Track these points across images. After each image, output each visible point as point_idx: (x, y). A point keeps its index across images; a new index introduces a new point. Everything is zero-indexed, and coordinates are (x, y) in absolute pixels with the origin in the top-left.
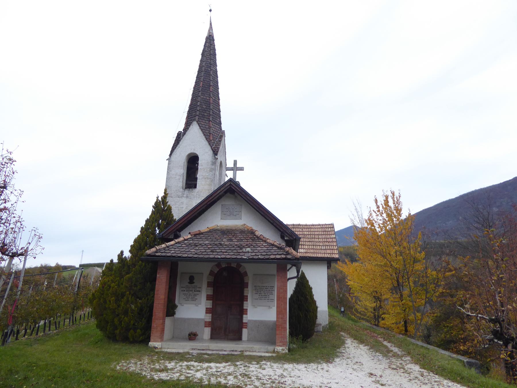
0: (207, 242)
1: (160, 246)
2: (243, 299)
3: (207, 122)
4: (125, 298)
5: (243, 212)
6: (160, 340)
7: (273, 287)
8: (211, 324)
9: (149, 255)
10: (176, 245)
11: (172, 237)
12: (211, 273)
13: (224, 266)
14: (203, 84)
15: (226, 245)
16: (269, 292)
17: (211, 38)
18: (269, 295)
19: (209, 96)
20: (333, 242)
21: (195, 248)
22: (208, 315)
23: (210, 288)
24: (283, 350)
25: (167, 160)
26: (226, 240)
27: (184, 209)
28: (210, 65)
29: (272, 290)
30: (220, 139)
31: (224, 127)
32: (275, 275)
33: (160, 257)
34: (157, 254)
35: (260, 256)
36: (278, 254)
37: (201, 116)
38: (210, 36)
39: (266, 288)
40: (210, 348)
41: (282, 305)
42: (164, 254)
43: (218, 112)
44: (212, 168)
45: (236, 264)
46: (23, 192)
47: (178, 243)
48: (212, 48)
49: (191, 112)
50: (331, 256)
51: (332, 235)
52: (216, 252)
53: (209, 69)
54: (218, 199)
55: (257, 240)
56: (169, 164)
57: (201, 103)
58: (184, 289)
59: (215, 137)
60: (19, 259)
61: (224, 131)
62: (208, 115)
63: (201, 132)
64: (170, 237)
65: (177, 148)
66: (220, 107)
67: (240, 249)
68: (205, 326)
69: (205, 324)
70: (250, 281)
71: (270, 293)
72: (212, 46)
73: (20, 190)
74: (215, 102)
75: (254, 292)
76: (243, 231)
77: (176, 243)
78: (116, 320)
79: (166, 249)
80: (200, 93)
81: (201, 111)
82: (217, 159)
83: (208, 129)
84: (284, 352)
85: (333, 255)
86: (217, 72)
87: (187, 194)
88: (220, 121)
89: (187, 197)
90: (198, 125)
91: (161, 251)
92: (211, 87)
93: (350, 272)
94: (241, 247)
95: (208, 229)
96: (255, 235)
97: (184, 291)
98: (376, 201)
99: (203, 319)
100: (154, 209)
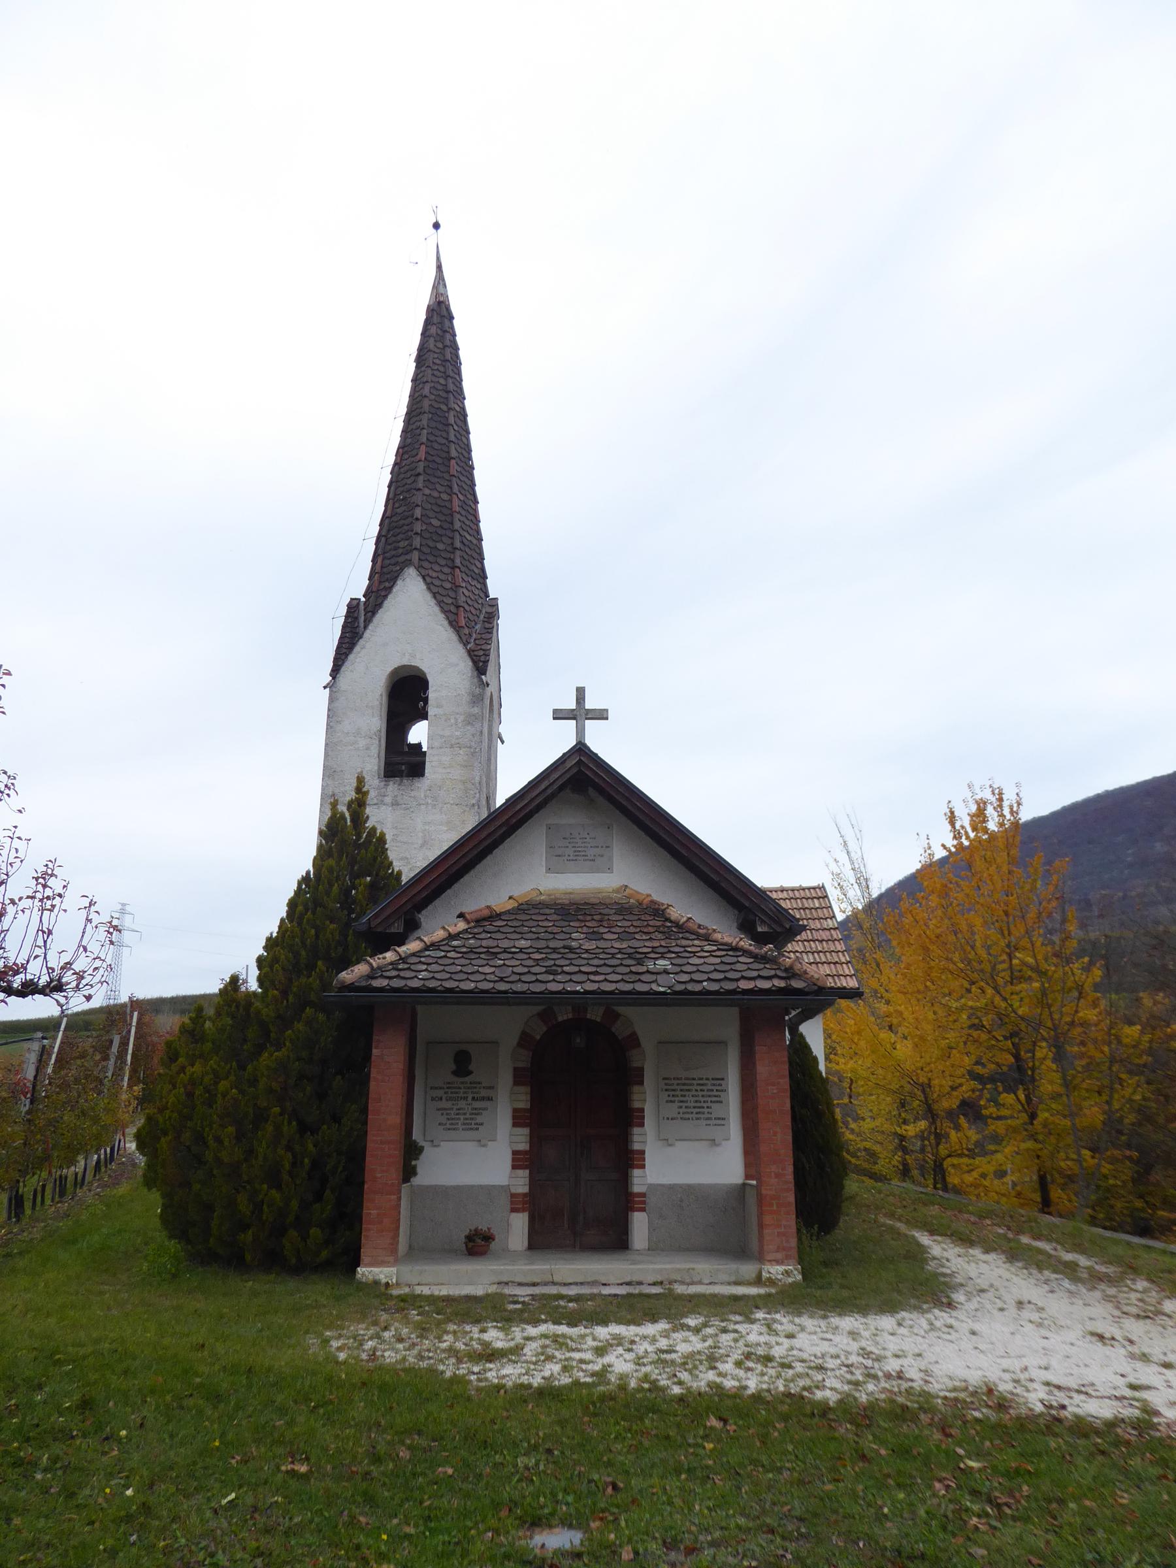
0: (523, 943)
1: (381, 956)
2: (630, 1118)
3: (446, 570)
4: (270, 1128)
5: (615, 850)
6: (391, 1259)
7: (723, 1079)
8: (530, 1203)
9: (352, 987)
10: (427, 953)
12: (525, 1040)
13: (565, 1018)
15: (587, 951)
16: (710, 1096)
17: (445, 313)
18: (709, 1104)
19: (449, 491)
20: (833, 941)
21: (491, 963)
22: (520, 1172)
23: (522, 1089)
24: (789, 1276)
26: (582, 936)
28: (444, 395)
30: (487, 625)
31: (494, 588)
33: (405, 991)
34: (377, 983)
35: (705, 984)
36: (760, 977)
38: (440, 303)
39: (698, 1085)
40: (557, 1279)
41: (775, 1134)
42: (396, 983)
43: (475, 541)
45: (601, 1010)
46: (15, 778)
48: (448, 343)
49: (394, 539)
50: (836, 983)
51: (826, 919)
52: (563, 972)
53: (444, 408)
55: (681, 935)
56: (332, 700)
58: (440, 1093)
59: (471, 617)
60: (57, 1001)
61: (497, 599)
62: (449, 549)
63: (433, 602)
66: (481, 524)
67: (639, 964)
68: (513, 1210)
69: (512, 1203)
70: (649, 1063)
71: (714, 1099)
72: (448, 336)
73: (5, 773)
75: (664, 1096)
76: (627, 906)
77: (427, 948)
78: (242, 1201)
79: (400, 967)
80: (421, 478)
81: (427, 535)
82: (488, 685)
83: (452, 594)
84: (790, 1280)
85: (840, 980)
86: (465, 416)
88: (483, 570)
89: (395, 804)
90: (420, 579)
91: (384, 974)
92: (453, 462)
93: (846, 1033)
94: (638, 956)
95: (511, 901)
96: (668, 920)
98: (952, 819)
99: (502, 1187)
100: (324, 842)
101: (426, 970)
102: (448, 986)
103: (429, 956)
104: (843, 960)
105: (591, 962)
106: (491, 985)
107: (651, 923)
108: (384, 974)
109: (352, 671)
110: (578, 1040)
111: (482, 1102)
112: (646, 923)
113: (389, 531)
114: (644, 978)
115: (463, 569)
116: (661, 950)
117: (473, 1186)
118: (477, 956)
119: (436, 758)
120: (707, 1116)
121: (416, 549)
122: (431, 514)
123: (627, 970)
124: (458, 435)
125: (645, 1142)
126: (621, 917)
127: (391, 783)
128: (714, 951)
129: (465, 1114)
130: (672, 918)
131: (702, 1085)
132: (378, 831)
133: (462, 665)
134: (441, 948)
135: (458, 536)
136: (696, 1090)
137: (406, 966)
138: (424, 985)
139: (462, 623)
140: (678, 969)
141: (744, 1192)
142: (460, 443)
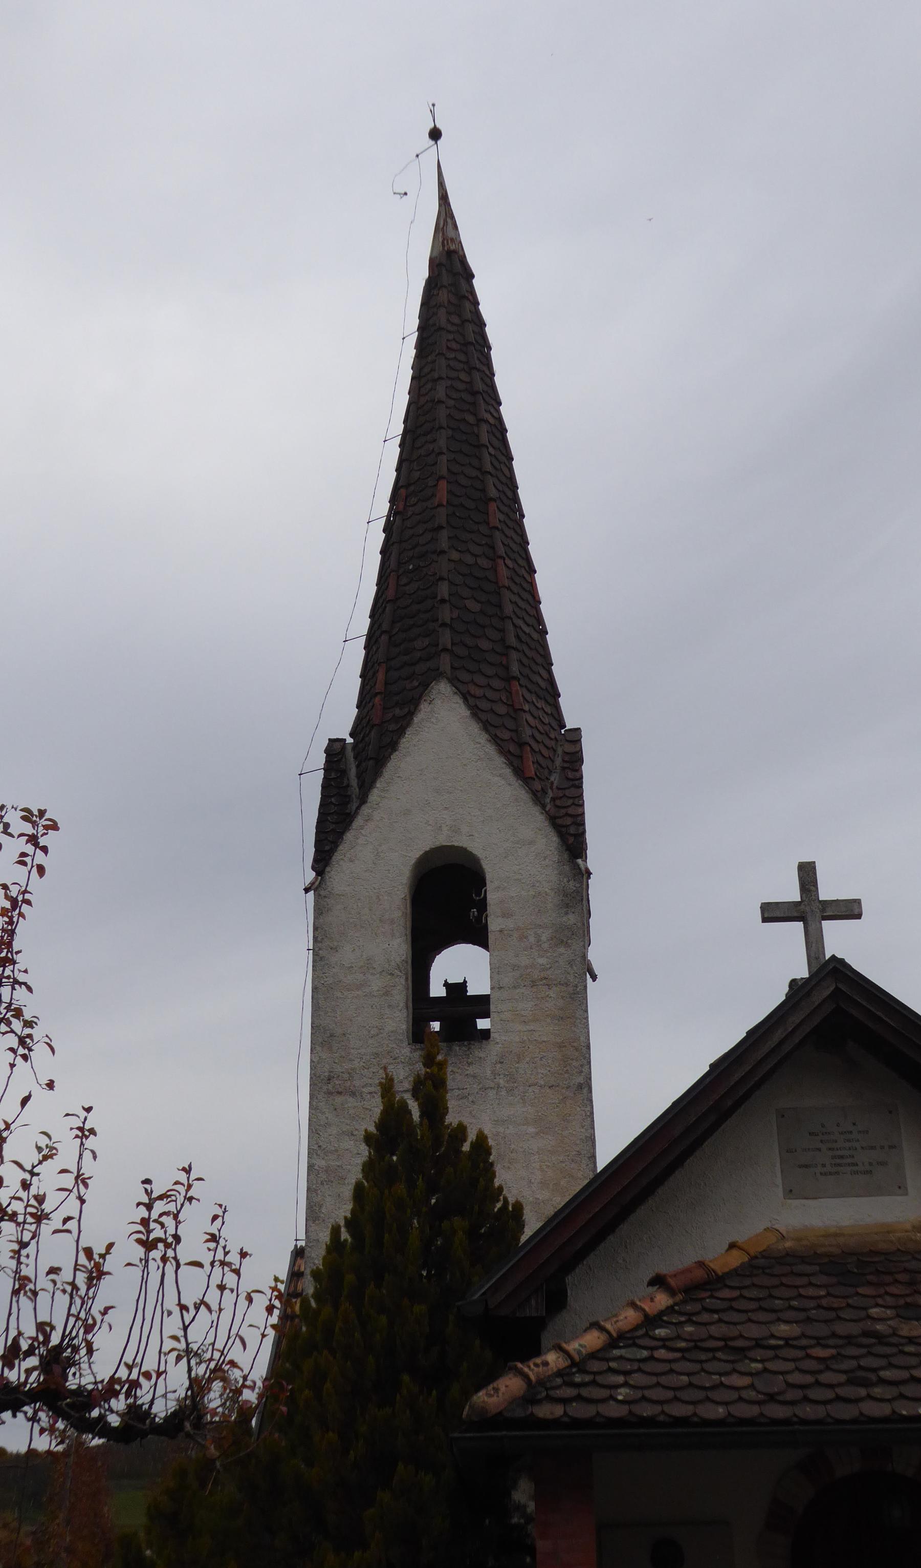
1: (538, 1361)
3: (497, 683)
10: (616, 1352)
14: (450, 492)
25: (307, 890)
34: (545, 1411)
43: (535, 636)
48: (469, 316)
53: (471, 419)
56: (319, 911)
61: (577, 731)
63: (483, 738)
72: (467, 305)
74: (517, 580)
80: (444, 534)
83: (510, 724)
90: (458, 699)
95: (735, 1252)
101: (626, 1384)
103: (621, 1358)
106: (657, 1409)
108: (552, 1393)
109: (351, 861)
113: (393, 622)
115: (523, 681)
118: (710, 1355)
121: (445, 650)
124: (496, 463)
132: (472, 1136)
134: (639, 1342)
135: (511, 627)
137: (588, 1378)
138: (762, 1414)
139: (531, 770)
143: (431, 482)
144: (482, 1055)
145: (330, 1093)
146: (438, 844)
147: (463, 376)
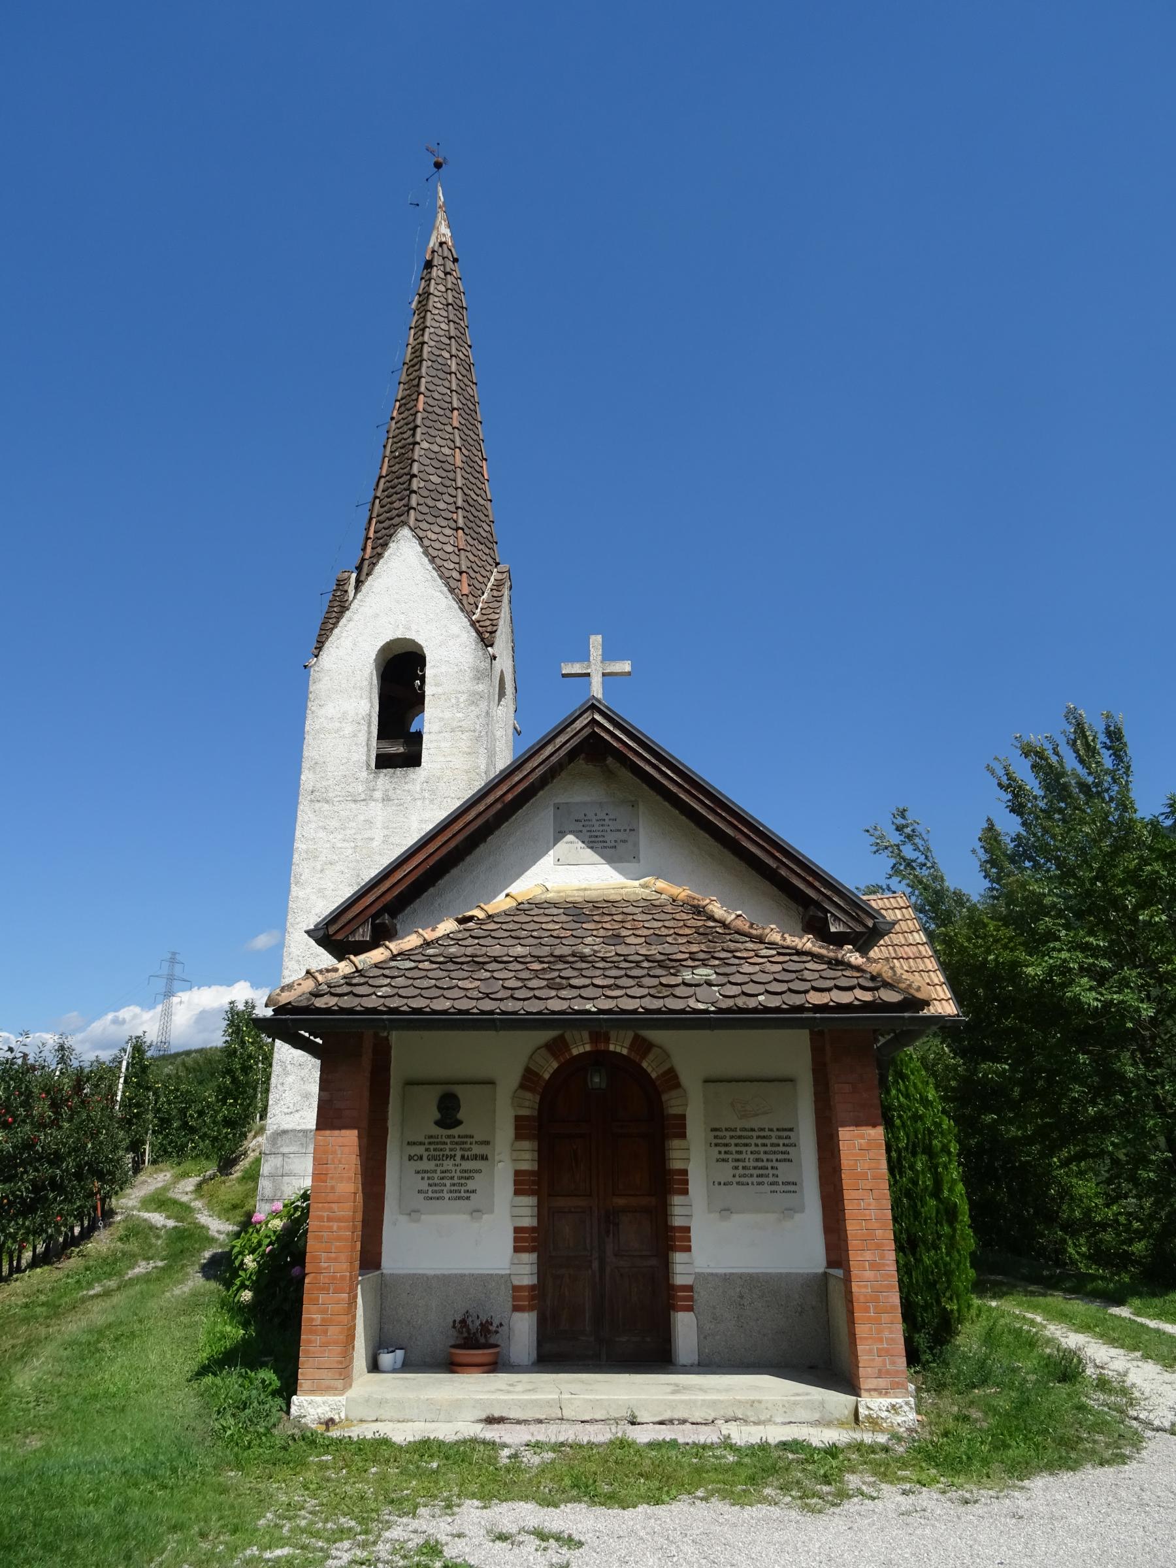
3: (448, 531)
5: (641, 830)
7: (791, 1130)
10: (393, 964)
11: (364, 934)
12: (529, 1079)
13: (581, 1050)
15: (603, 959)
16: (775, 1153)
18: (775, 1164)
23: (526, 1144)
24: (897, 1413)
27: (375, 844)
29: (786, 1141)
30: (495, 593)
32: (790, 1080)
34: (320, 1003)
35: (761, 998)
37: (424, 509)
39: (758, 1137)
40: (567, 1414)
44: (475, 693)
47: (399, 954)
54: (544, 781)
55: (728, 937)
57: (422, 468)
58: (420, 1150)
64: (358, 937)
65: (341, 624)
68: (517, 1309)
69: (514, 1298)
71: (780, 1157)
77: (394, 958)
79: (355, 981)
81: (426, 493)
87: (387, 790)
89: (386, 799)
95: (508, 899)
97: (421, 1158)
99: (502, 1276)
101: (389, 985)
102: (414, 1006)
104: (936, 981)
105: (607, 973)
107: (689, 923)
110: (597, 1080)
111: (474, 1162)
112: (682, 923)
114: (679, 991)
115: (467, 530)
116: (702, 956)
117: (463, 1276)
119: (435, 744)
120: (771, 1179)
122: (430, 470)
123: (655, 982)
125: (689, 1216)
126: (650, 917)
127: (382, 775)
128: (773, 956)
129: (452, 1178)
130: (717, 916)
131: (764, 1137)
133: (464, 635)
136: (756, 1145)
137: (362, 980)
140: (723, 980)
141: (826, 1284)
142: (465, 393)
143: (414, 397)
144: (414, 777)
145: (312, 801)
146: (395, 637)
147: (444, 326)
